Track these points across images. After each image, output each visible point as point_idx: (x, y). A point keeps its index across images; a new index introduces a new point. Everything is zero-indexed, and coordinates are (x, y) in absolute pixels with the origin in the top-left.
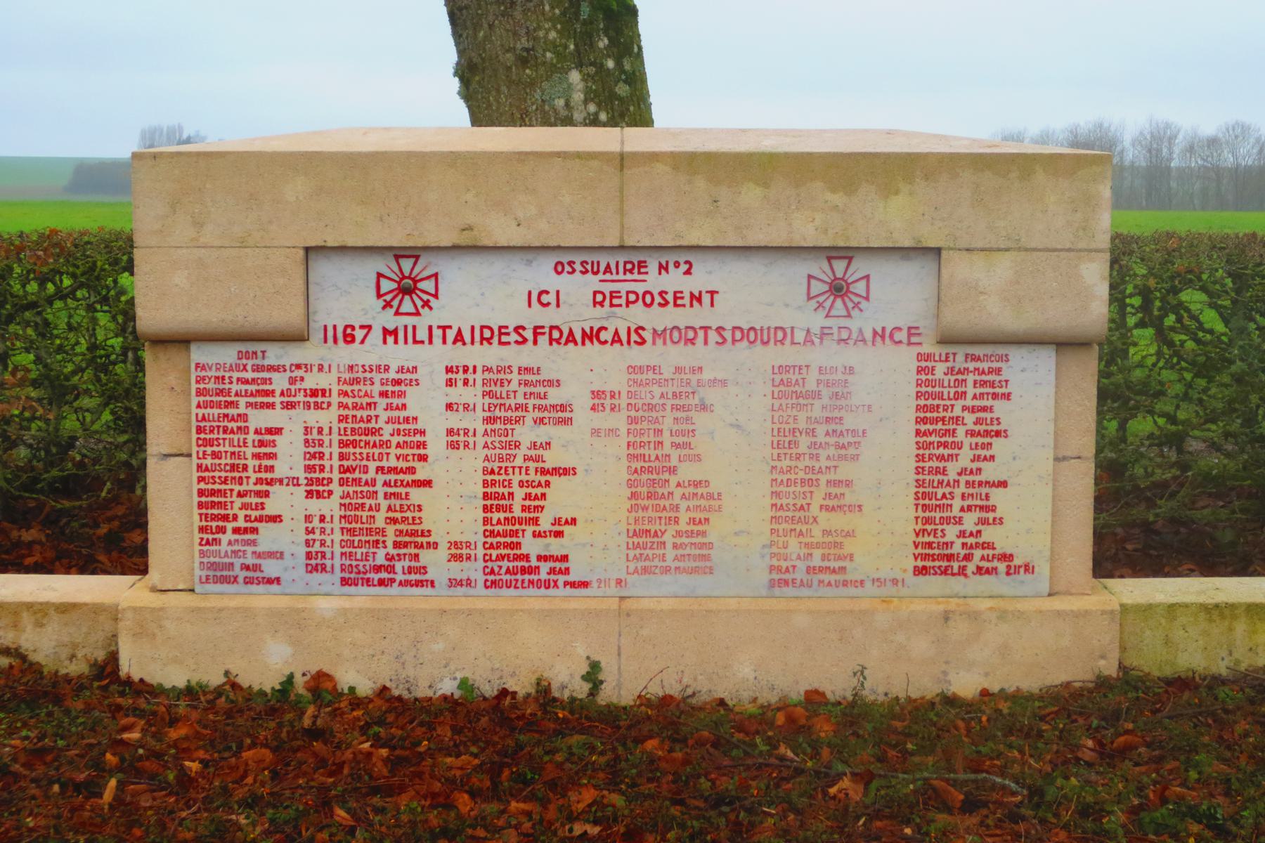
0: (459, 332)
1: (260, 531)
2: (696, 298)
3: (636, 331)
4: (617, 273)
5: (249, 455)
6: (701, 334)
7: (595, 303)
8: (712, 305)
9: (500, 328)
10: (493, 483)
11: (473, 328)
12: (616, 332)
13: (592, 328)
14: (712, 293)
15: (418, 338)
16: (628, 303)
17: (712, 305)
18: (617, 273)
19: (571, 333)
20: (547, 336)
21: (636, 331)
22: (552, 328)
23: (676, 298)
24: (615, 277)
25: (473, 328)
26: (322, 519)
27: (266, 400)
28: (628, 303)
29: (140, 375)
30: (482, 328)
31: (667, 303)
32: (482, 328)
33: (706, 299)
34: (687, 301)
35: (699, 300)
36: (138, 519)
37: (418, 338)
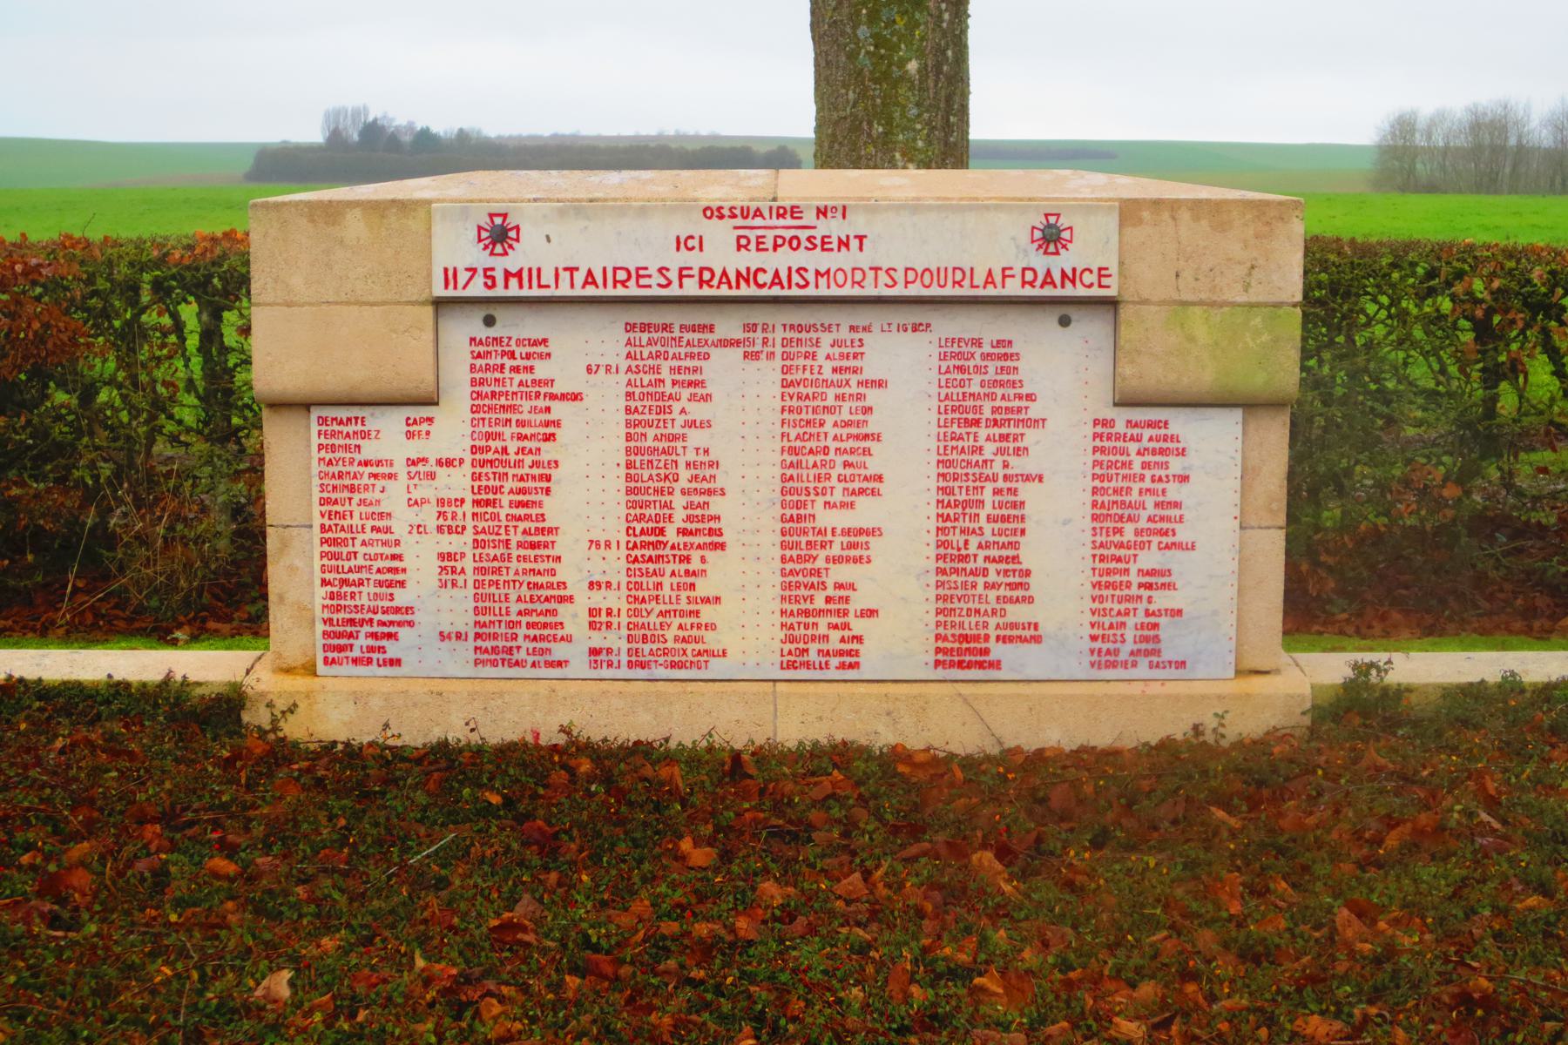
0: (590, 273)
1: (400, 636)
2: (844, 244)
3: (798, 271)
4: (605, 285)
5: (507, 435)
6: (871, 274)
7: (739, 247)
8: (861, 249)
9: (638, 269)
10: (1104, 491)
11: (605, 270)
12: (777, 274)
13: (748, 269)
14: (861, 238)
15: (543, 282)
16: (776, 247)
17: (861, 249)
18: (605, 285)
19: (724, 273)
20: (697, 278)
21: (798, 271)
22: (702, 270)
23: (823, 243)
24: (601, 292)
25: (605, 270)
26: (609, 613)
27: (336, 642)
28: (776, 247)
29: (859, 765)
30: (615, 269)
31: (815, 246)
32: (615, 269)
33: (854, 243)
34: (835, 245)
35: (847, 245)
36: (857, 162)
37: (543, 282)
